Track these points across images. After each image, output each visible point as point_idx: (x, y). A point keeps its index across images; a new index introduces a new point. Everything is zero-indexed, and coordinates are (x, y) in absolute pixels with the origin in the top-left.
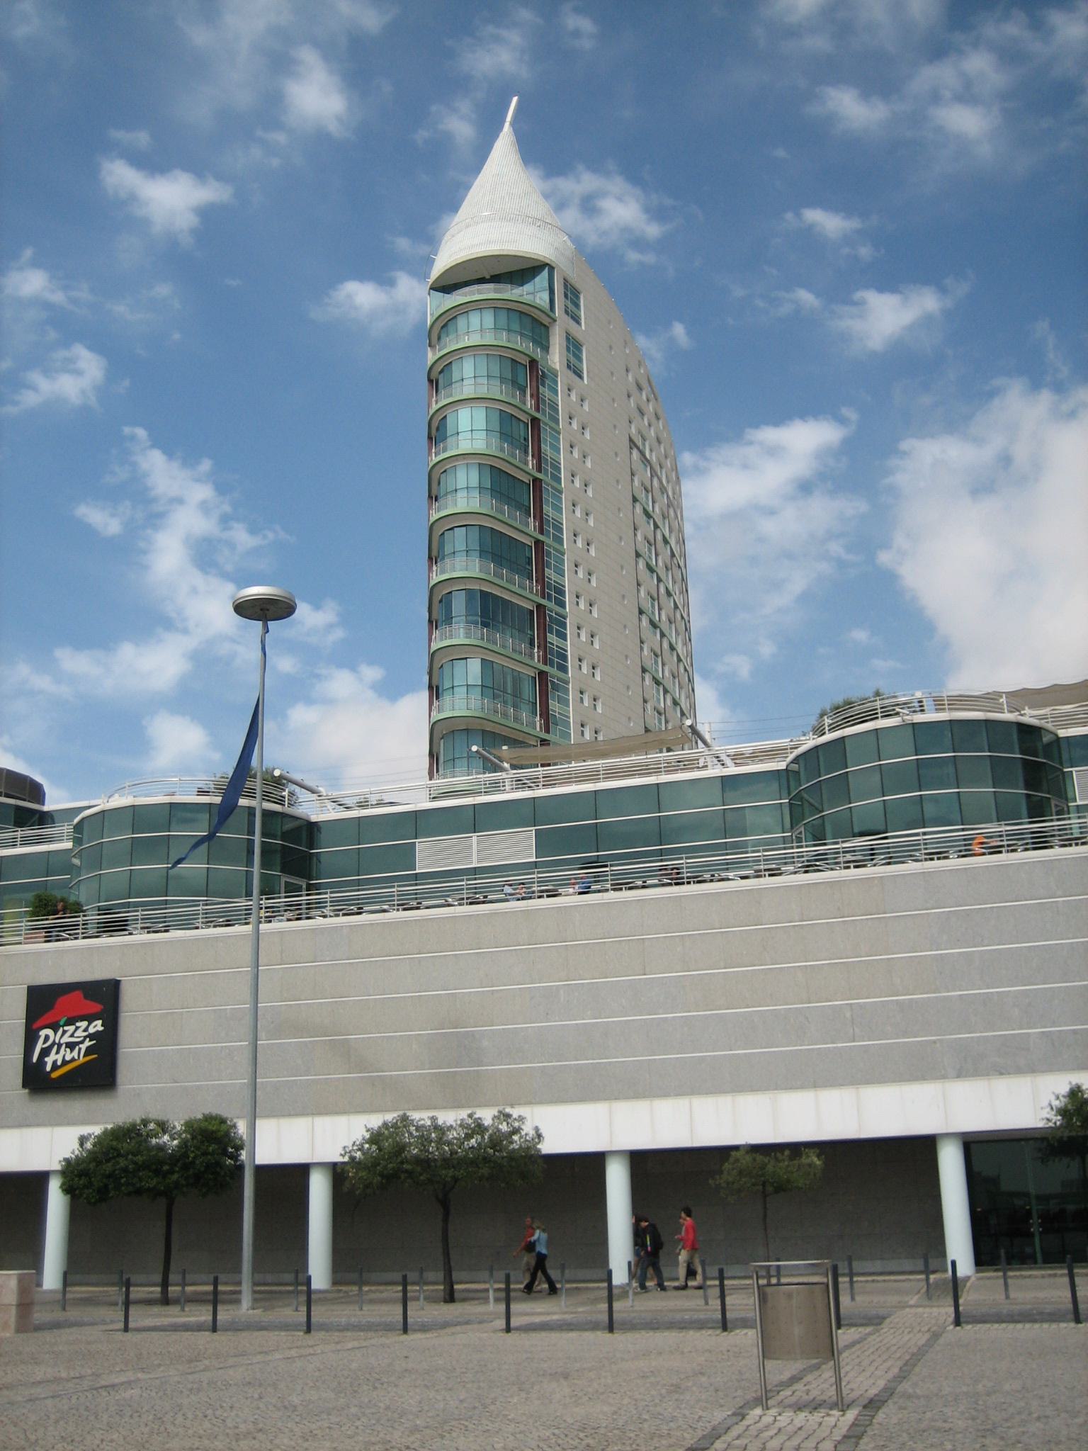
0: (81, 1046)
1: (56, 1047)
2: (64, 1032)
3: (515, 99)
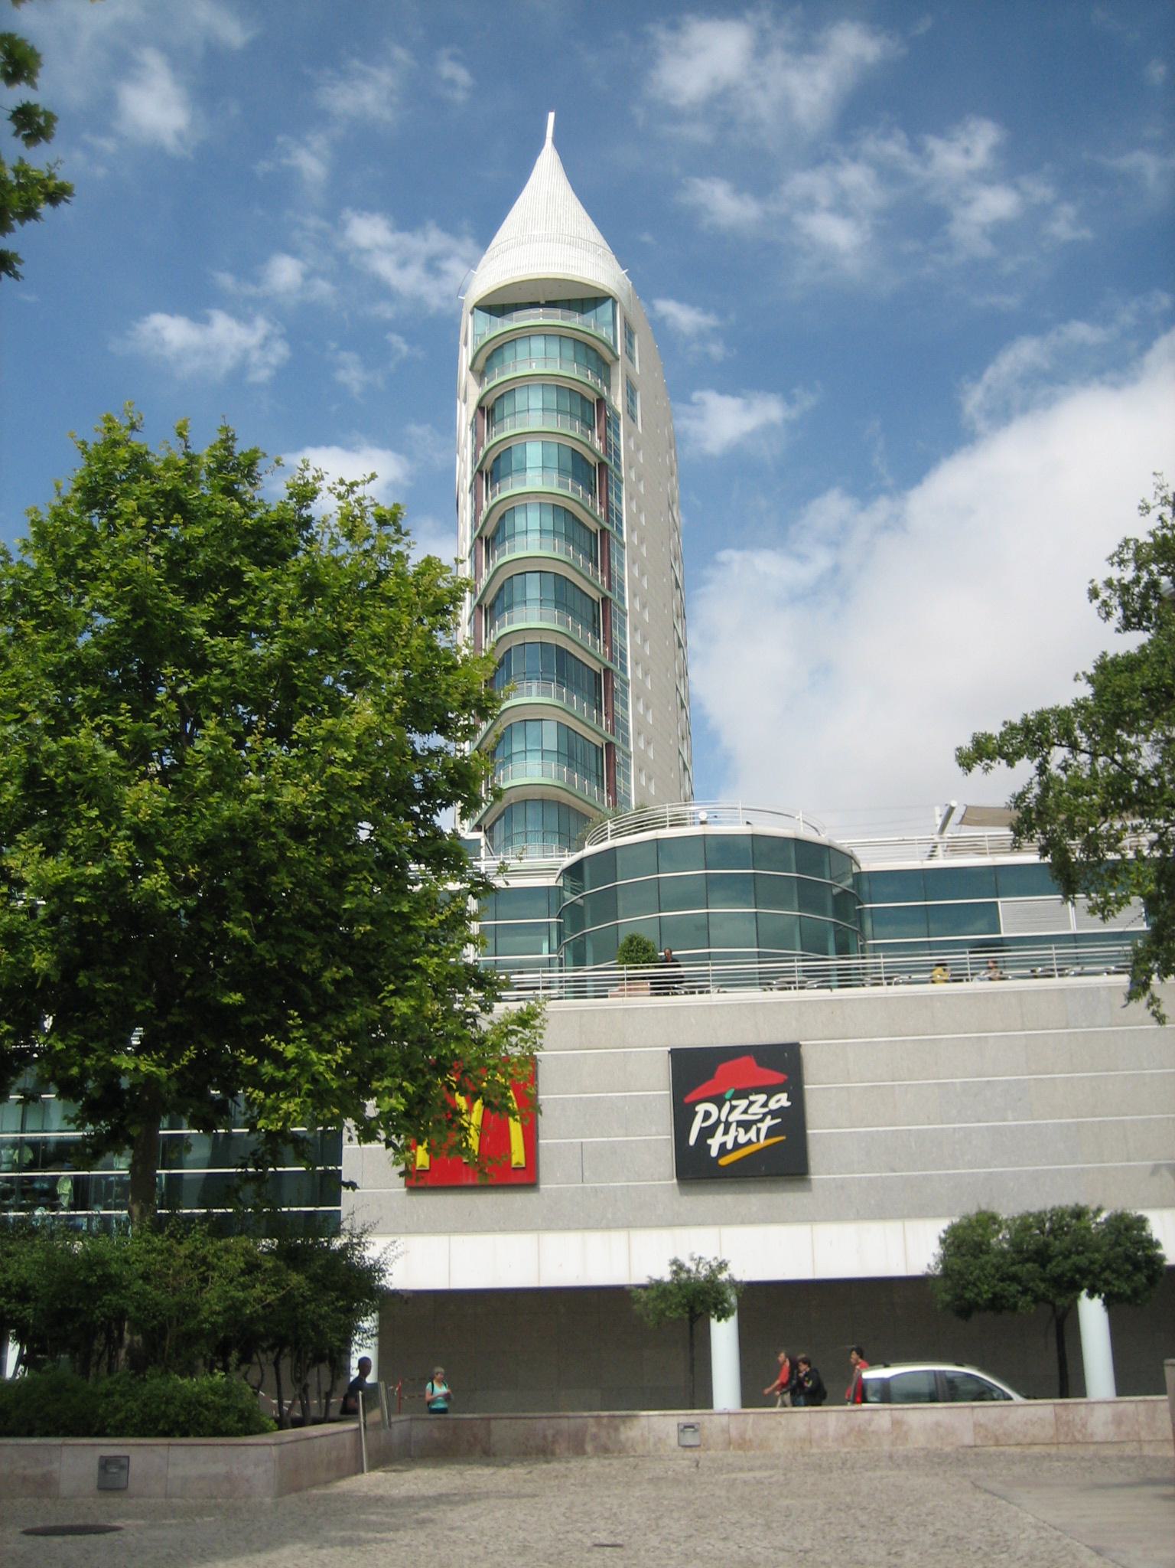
0: (759, 1125)
1: (721, 1127)
2: (733, 1108)
3: (551, 116)
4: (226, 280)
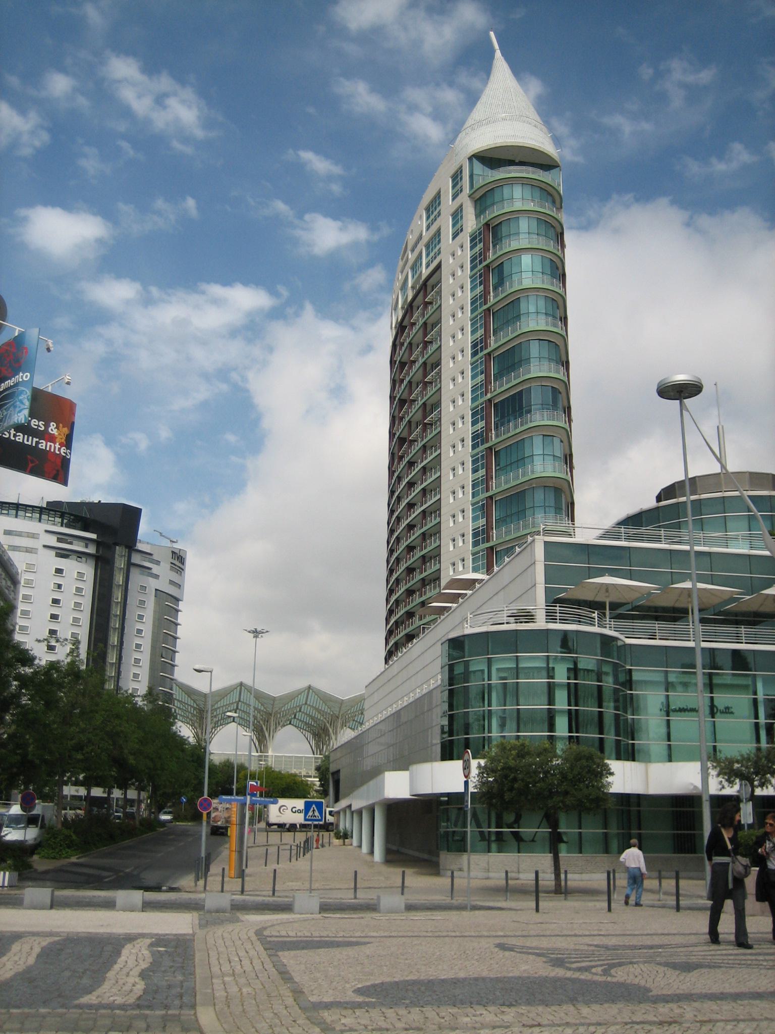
4: (13, 81)
